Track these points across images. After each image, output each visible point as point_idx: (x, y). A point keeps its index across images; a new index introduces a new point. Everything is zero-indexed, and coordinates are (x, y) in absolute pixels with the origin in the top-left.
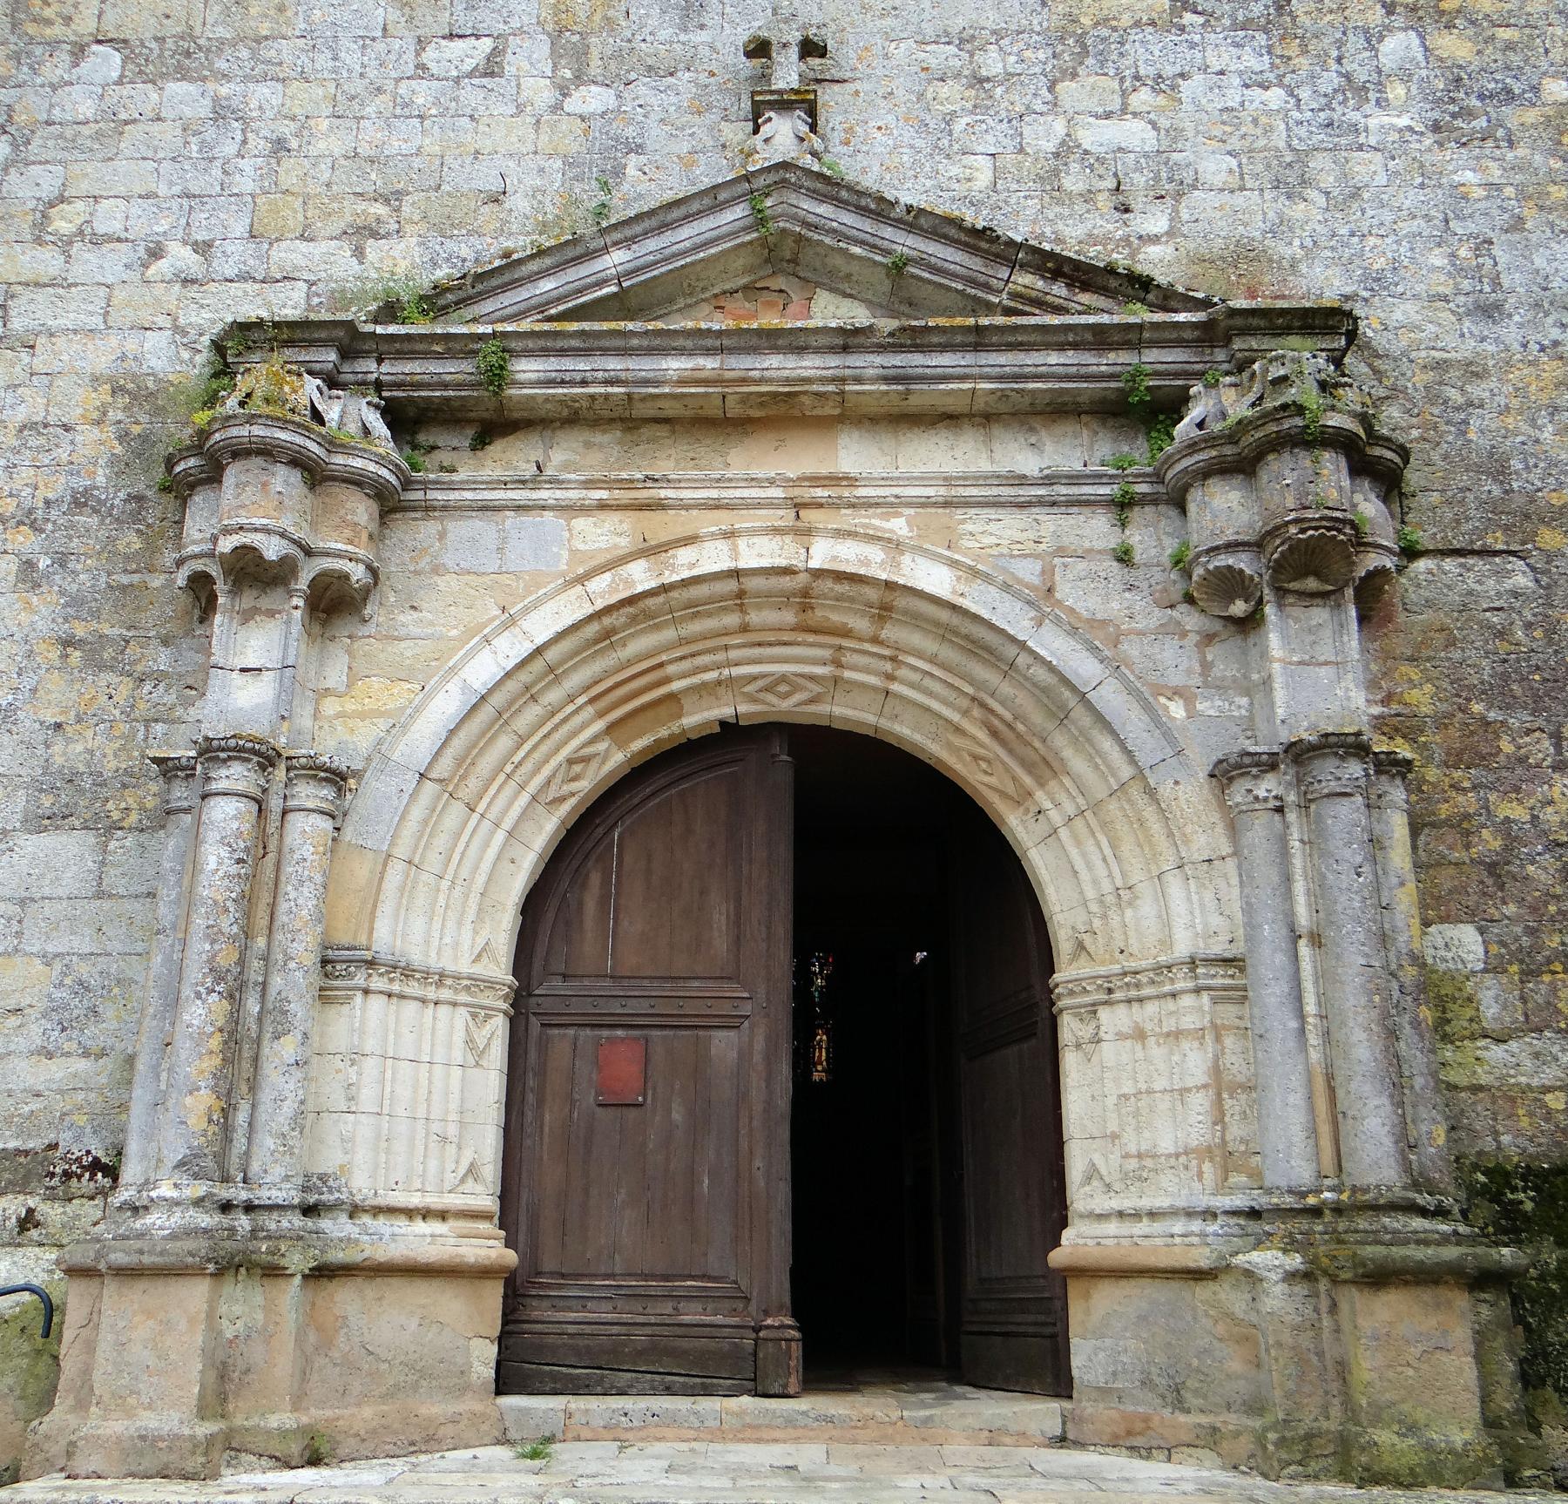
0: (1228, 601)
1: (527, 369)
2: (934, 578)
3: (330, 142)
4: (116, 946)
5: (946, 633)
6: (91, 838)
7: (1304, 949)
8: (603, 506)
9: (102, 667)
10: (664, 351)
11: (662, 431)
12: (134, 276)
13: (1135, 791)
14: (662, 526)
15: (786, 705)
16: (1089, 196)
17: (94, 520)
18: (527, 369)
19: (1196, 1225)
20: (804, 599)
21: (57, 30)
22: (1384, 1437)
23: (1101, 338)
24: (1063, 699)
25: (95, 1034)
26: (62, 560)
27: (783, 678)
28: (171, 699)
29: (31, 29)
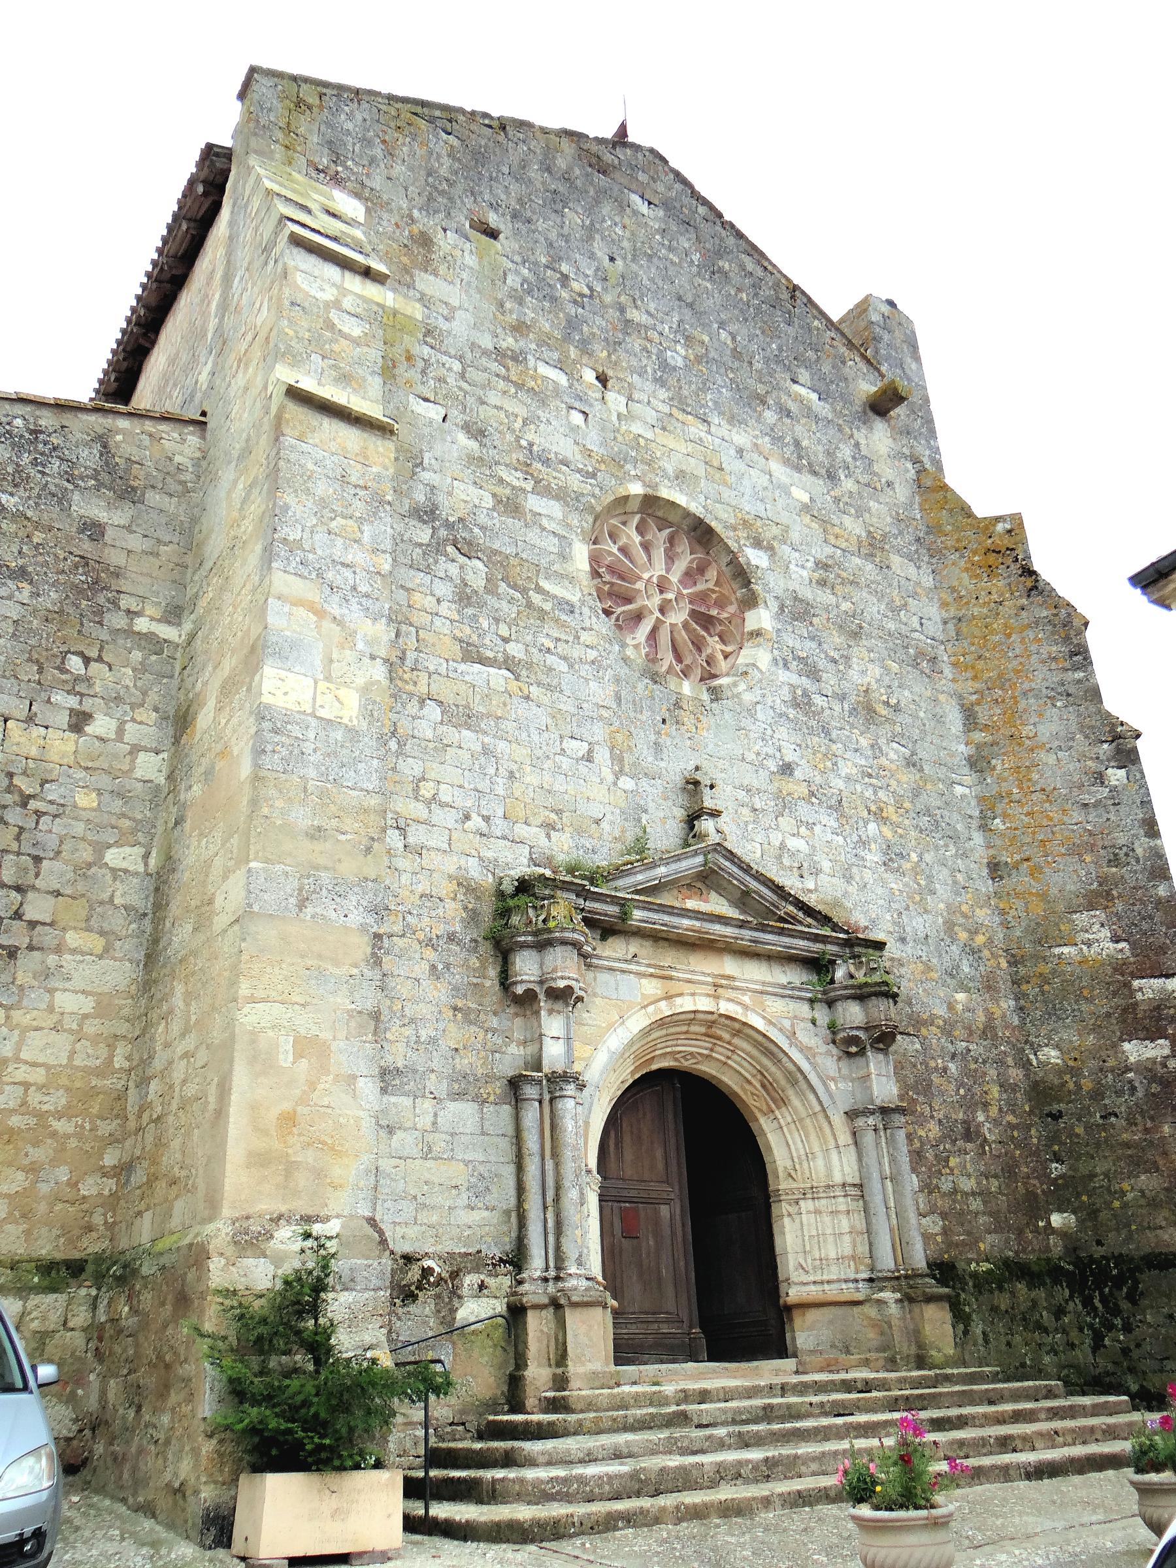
0: (851, 1047)
1: (638, 914)
2: (759, 1023)
3: (532, 779)
4: (493, 1159)
5: (757, 1044)
6: (476, 1106)
7: (888, 1183)
8: (651, 975)
9: (471, 1023)
10: (683, 916)
11: (666, 944)
12: (459, 827)
13: (821, 1117)
14: (675, 987)
15: (686, 1064)
16: (791, 868)
17: (458, 949)
18: (638, 914)
19: (851, 1285)
21: (410, 687)
22: (933, 1353)
23: (816, 938)
24: (796, 1077)
25: (491, 1199)
26: (447, 966)
27: (691, 1054)
28: (500, 1041)
29: (400, 683)
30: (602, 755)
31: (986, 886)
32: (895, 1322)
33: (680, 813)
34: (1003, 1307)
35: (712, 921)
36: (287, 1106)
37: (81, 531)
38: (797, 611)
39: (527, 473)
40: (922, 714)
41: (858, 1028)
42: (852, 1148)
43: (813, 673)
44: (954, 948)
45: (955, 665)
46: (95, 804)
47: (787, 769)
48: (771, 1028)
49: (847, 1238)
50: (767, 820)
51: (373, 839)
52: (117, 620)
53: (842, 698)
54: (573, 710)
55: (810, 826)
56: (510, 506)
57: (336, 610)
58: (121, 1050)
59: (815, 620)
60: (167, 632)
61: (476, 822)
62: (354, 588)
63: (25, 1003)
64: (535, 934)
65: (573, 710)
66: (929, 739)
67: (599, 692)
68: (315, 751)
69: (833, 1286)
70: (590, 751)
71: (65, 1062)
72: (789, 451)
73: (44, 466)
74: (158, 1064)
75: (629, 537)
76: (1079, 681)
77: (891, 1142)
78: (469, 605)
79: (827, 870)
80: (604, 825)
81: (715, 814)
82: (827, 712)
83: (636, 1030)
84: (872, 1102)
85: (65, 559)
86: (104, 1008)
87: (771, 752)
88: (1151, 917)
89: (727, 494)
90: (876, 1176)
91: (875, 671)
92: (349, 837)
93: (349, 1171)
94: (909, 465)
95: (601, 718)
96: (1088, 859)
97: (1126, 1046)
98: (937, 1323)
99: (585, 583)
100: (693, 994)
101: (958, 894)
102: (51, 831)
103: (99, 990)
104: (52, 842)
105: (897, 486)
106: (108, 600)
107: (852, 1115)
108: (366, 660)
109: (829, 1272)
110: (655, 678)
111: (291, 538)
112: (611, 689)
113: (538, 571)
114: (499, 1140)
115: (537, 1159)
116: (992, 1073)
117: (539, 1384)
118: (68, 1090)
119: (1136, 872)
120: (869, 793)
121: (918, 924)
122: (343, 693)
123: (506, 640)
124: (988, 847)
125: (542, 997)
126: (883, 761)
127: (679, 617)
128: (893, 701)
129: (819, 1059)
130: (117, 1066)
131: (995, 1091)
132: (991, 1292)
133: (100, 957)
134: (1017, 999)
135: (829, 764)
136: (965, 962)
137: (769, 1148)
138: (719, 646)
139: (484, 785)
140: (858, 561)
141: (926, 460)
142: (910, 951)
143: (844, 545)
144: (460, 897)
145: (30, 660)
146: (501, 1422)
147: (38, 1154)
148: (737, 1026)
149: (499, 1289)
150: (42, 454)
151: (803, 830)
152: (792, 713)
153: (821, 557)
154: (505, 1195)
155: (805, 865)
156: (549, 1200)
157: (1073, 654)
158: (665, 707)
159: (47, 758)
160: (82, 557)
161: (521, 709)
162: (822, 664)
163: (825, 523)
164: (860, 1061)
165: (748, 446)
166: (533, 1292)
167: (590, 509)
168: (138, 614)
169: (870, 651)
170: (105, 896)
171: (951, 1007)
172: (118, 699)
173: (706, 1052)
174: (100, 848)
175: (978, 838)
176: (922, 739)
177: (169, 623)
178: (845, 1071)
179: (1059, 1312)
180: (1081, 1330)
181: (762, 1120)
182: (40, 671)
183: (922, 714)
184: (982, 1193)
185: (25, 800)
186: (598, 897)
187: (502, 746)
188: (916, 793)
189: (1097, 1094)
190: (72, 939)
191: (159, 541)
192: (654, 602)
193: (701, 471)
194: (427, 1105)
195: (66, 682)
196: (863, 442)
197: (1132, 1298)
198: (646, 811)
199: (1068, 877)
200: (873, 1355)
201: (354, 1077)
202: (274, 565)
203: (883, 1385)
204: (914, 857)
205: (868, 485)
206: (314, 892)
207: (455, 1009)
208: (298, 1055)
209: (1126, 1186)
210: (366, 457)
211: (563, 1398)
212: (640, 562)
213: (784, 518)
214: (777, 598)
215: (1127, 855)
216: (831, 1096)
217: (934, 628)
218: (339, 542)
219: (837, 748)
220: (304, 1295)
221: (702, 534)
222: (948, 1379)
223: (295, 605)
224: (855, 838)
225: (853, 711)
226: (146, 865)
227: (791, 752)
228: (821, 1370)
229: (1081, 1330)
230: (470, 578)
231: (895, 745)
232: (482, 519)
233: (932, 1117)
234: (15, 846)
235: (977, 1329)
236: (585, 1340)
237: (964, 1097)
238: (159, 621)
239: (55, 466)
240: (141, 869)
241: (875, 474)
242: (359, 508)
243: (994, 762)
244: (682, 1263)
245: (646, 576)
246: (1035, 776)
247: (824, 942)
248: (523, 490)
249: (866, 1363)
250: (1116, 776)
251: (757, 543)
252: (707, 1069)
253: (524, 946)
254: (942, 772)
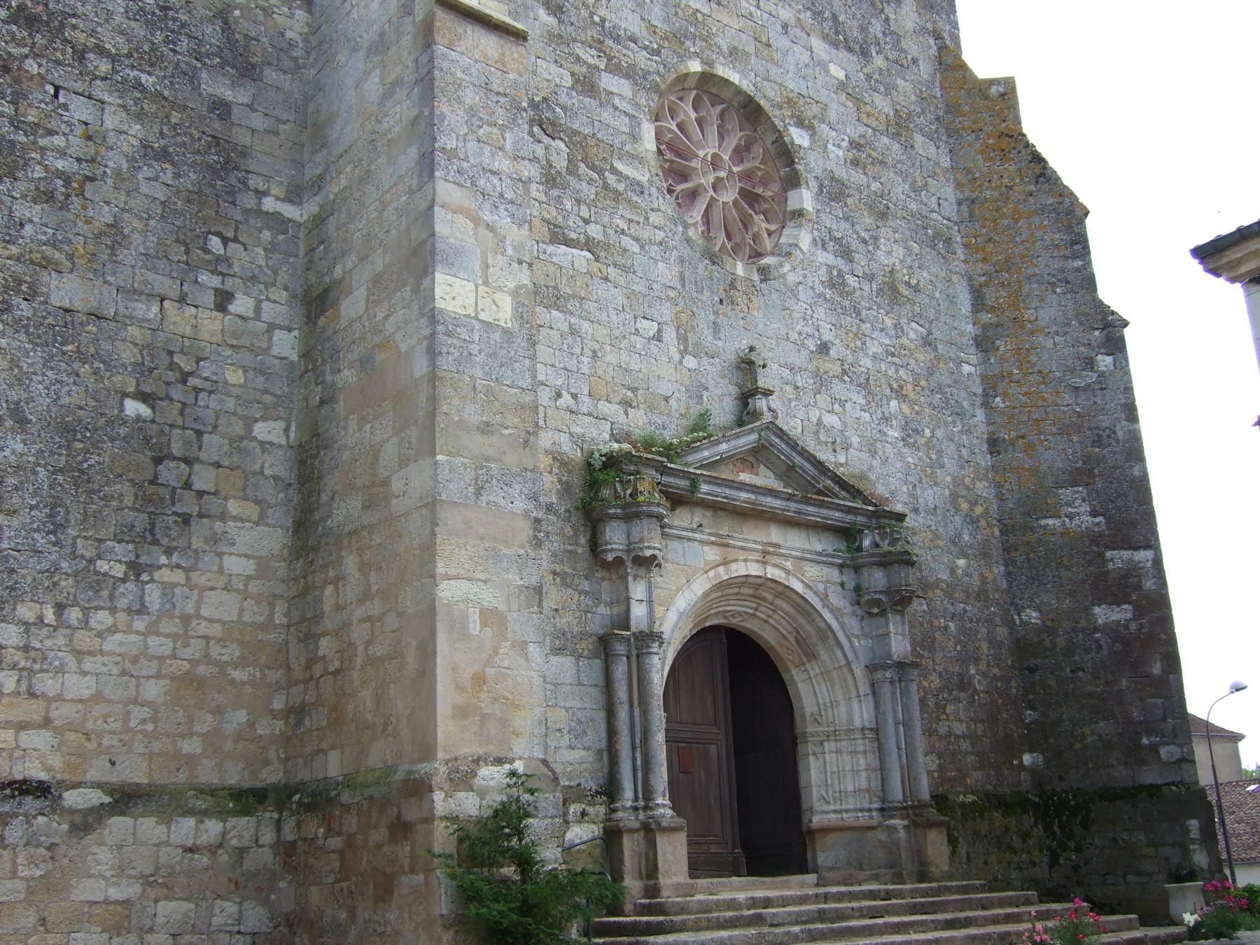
1: (704, 488)
2: (798, 586)
4: (587, 706)
5: (795, 605)
8: (713, 543)
9: (568, 586)
11: (723, 514)
13: (845, 670)
14: (732, 554)
15: (734, 621)
17: (554, 518)
18: (704, 488)
20: (758, 587)
22: (932, 869)
23: (849, 510)
24: (826, 634)
30: (670, 335)
31: (985, 461)
32: (903, 844)
33: (734, 390)
34: (983, 832)
35: (764, 495)
36: (478, 668)
37: (211, 111)
38: (833, 191)
39: (600, 50)
40: (937, 295)
41: (881, 592)
42: (870, 698)
43: (846, 253)
44: (957, 518)
45: (966, 246)
46: (242, 381)
47: (824, 348)
48: (808, 591)
49: (864, 774)
50: (807, 398)
51: (528, 432)
52: (249, 201)
53: (871, 278)
54: (645, 291)
55: (842, 403)
56: (586, 85)
57: (487, 217)
58: (280, 608)
59: (849, 201)
60: (290, 211)
61: (566, 399)
62: (501, 195)
63: (200, 565)
64: (624, 507)
65: (645, 291)
66: (942, 319)
67: (666, 272)
68: (480, 351)
69: (850, 815)
70: (659, 331)
71: (235, 618)
72: (827, 25)
73: (175, 44)
74: (328, 624)
75: (686, 114)
76: (1078, 270)
77: (905, 693)
78: (554, 186)
79: (856, 445)
80: (672, 402)
81: (767, 393)
82: (858, 292)
83: (700, 593)
84: (890, 658)
85: (200, 139)
86: (263, 570)
87: (810, 332)
88: (1125, 495)
89: (774, 71)
90: (890, 721)
91: (899, 251)
92: (510, 431)
93: (525, 721)
94: (932, 41)
95: (668, 299)
96: (1075, 439)
97: (1097, 610)
98: (936, 845)
99: (653, 163)
100: (745, 560)
101: (962, 467)
102: (209, 405)
103: (258, 554)
104: (209, 416)
105: (921, 63)
106: (239, 180)
107: (871, 668)
108: (515, 265)
109: (847, 803)
110: (714, 259)
111: (448, 147)
112: (676, 270)
113: (612, 152)
114: (592, 689)
115: (626, 707)
116: (984, 631)
117: (634, 893)
118: (241, 643)
119: (1115, 453)
120: (891, 372)
121: (929, 496)
122: (498, 296)
123: (587, 222)
124: (988, 424)
125: (629, 564)
126: (905, 341)
127: (729, 196)
128: (914, 282)
129: (846, 619)
130: (277, 622)
131: (985, 646)
132: (974, 819)
133: (257, 523)
134: (1006, 565)
135: (859, 343)
136: (966, 531)
137: (799, 696)
138: (764, 225)
139: (572, 364)
140: (886, 140)
141: (946, 35)
142: (921, 521)
143: (874, 124)
144: (556, 470)
145: (177, 241)
146: (609, 922)
147: (220, 699)
148: (780, 589)
149: (597, 815)
150: (173, 31)
151: (836, 406)
152: (828, 293)
153: (855, 136)
154: (596, 736)
155: (838, 440)
156: (638, 741)
157: (1074, 243)
158: (721, 287)
159: (200, 337)
160: (213, 137)
161: (601, 291)
162: (855, 244)
163: (858, 101)
164: (881, 620)
165: (792, 21)
166: (626, 818)
167: (655, 88)
168: (265, 194)
169: (895, 232)
170: (257, 467)
171: (953, 572)
172: (254, 279)
173: (751, 611)
174: (250, 422)
175: (980, 415)
176: (937, 319)
177: (291, 202)
178: (866, 630)
179: (1025, 836)
180: (1041, 851)
181: (794, 672)
182: (187, 252)
183: (937, 295)
184: (971, 737)
185: (185, 377)
186: (673, 473)
187: (586, 325)
188: (931, 372)
189: (1069, 650)
190: (234, 507)
191: (278, 120)
192: (707, 180)
193: (750, 48)
195: (209, 262)
196: (892, 16)
197: (1084, 825)
198: (706, 389)
199: (1056, 454)
200: (883, 871)
201: (526, 643)
202: (437, 174)
203: (900, 894)
204: (927, 432)
205: (896, 62)
206: (487, 481)
207: (554, 573)
208: (484, 625)
209: (1087, 731)
210: (504, 64)
211: (659, 904)
212: (695, 139)
213: (823, 96)
214: (816, 178)
215: (1109, 436)
216: (855, 652)
217: (950, 209)
218: (487, 150)
219: (866, 327)
220: (508, 818)
221: (750, 112)
222: (948, 890)
223: (455, 212)
224: (879, 415)
225: (880, 292)
226: (288, 437)
227: (827, 332)
228: (839, 884)
229: (1041, 851)
230: (554, 158)
231: (914, 325)
232: (563, 98)
233: (934, 670)
234: (180, 421)
235: (962, 850)
236: (671, 858)
237: (960, 652)
238: (283, 200)
239: (184, 44)
240: (284, 442)
241: (902, 50)
242: (501, 116)
243: (998, 343)
244: (727, 795)
245: (701, 154)
246: (1034, 359)
247: (855, 514)
248: (597, 68)
249: (876, 878)
250: (1104, 362)
251: (800, 123)
252: (750, 626)
253: (615, 517)
254: (953, 351)
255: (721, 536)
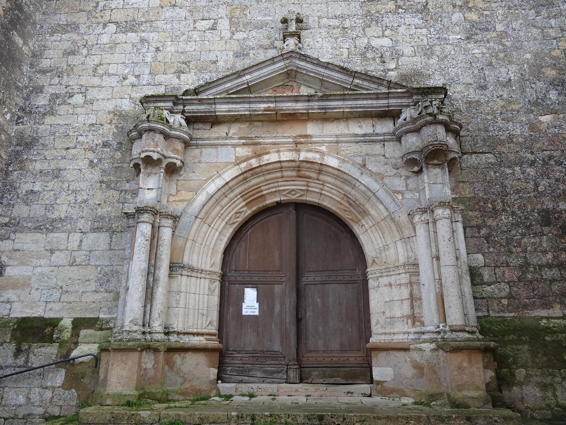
5: (336, 177)
11: (259, 124)
15: (294, 197)
20: (298, 169)
21: (100, 20)
23: (377, 97)
26: (100, 160)
27: (293, 190)
194: (77, 237)
255: (251, 138)
